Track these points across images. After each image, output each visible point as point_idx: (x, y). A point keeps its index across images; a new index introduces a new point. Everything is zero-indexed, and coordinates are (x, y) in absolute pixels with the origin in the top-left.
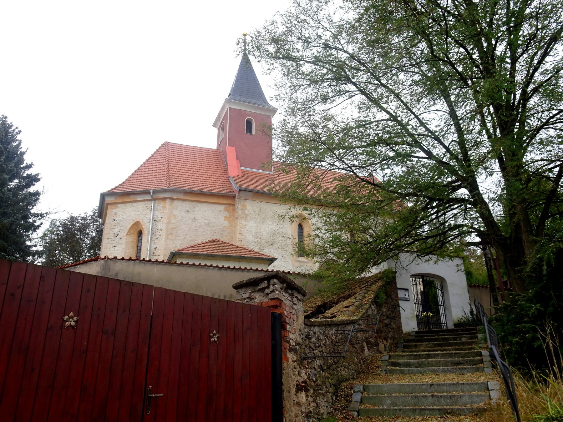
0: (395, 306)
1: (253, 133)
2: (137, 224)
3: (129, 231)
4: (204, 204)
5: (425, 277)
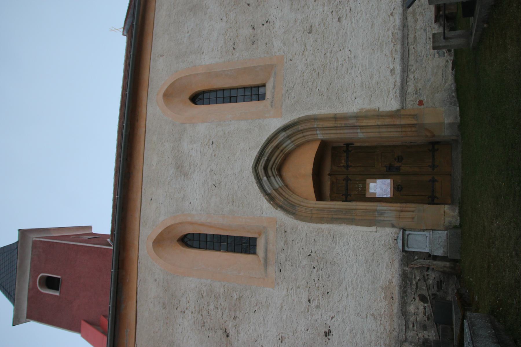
1: (59, 277)
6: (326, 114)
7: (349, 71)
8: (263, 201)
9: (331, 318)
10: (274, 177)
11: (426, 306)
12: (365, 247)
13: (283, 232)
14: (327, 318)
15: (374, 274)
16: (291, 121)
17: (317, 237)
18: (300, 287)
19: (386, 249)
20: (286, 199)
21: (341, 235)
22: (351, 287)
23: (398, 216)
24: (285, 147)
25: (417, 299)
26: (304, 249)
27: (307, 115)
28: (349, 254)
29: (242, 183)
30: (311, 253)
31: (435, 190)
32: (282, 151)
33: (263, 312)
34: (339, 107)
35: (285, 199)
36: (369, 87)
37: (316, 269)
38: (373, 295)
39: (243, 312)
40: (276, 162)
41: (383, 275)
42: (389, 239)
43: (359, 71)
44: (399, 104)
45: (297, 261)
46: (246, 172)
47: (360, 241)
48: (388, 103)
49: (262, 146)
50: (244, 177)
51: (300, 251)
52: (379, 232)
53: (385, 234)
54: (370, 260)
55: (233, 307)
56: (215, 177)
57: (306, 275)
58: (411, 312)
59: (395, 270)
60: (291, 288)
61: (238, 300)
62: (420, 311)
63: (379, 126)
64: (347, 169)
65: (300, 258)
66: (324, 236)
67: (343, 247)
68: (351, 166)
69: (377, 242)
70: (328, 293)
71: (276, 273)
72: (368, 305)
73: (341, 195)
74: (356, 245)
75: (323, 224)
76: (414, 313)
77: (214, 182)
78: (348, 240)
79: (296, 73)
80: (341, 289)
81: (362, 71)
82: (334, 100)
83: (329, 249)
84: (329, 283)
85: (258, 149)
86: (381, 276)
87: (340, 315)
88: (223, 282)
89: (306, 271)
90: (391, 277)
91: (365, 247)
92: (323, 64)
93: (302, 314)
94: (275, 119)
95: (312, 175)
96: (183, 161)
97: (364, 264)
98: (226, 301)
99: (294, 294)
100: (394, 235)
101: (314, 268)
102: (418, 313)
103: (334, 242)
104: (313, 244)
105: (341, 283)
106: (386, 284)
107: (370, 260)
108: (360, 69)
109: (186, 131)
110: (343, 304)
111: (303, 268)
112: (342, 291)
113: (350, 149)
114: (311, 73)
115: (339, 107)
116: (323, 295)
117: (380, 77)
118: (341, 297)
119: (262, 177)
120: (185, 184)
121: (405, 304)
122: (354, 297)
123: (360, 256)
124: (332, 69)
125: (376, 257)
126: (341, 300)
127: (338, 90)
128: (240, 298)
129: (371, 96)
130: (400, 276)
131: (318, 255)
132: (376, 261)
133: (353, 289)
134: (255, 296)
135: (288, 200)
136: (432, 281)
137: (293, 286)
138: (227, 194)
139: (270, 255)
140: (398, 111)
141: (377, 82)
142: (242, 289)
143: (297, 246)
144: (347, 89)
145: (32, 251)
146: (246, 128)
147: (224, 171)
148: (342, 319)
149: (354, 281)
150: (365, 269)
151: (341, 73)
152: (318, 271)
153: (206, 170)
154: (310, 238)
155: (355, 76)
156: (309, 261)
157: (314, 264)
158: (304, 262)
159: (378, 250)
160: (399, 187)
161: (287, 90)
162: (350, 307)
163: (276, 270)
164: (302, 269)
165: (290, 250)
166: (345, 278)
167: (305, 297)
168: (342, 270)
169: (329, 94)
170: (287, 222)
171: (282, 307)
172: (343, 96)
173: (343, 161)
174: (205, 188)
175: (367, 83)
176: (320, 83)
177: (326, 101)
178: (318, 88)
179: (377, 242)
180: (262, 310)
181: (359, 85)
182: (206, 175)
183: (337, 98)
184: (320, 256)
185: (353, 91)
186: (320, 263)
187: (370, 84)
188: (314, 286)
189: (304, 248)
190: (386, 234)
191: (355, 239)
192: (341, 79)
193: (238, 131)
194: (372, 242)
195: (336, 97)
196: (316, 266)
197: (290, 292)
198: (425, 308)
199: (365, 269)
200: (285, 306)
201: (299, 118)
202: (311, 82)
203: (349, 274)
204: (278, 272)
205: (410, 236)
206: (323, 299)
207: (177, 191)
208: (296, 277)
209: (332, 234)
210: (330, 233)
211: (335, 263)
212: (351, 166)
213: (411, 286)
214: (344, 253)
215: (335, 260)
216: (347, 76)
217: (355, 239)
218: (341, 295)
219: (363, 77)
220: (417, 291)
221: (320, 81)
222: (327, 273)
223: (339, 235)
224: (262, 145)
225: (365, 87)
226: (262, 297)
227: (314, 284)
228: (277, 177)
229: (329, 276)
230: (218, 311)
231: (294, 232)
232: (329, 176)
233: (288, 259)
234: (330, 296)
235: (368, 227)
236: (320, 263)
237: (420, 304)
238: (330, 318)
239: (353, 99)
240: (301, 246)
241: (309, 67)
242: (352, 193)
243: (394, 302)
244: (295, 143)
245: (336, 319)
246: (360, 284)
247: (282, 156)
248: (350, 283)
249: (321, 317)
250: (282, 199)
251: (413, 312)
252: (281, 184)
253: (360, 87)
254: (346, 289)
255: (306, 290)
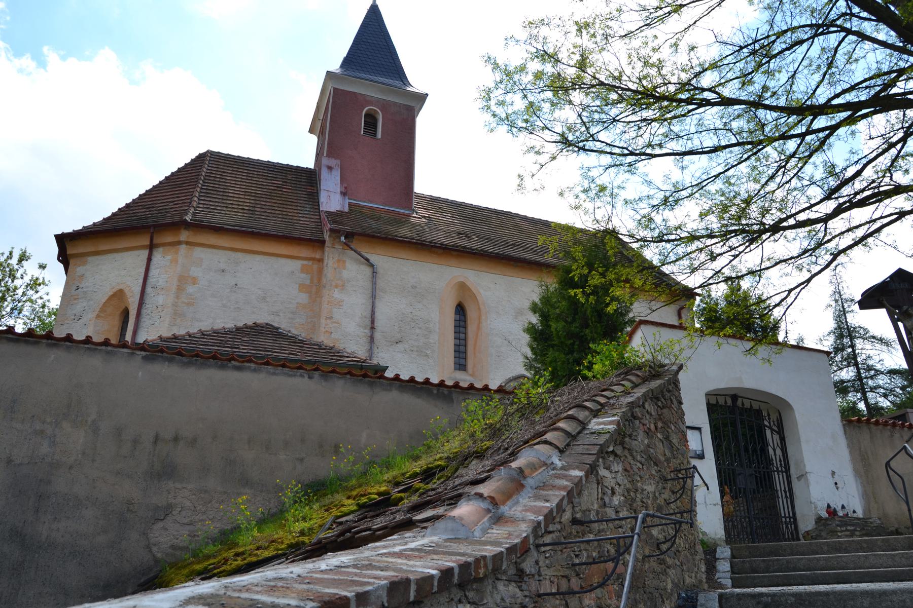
0: (679, 471)
1: (379, 135)
2: (119, 295)
3: (103, 309)
4: (258, 258)
5: (740, 400)
75: (863, 498)
128: (427, 356)
145: (404, 105)
182: (516, 335)
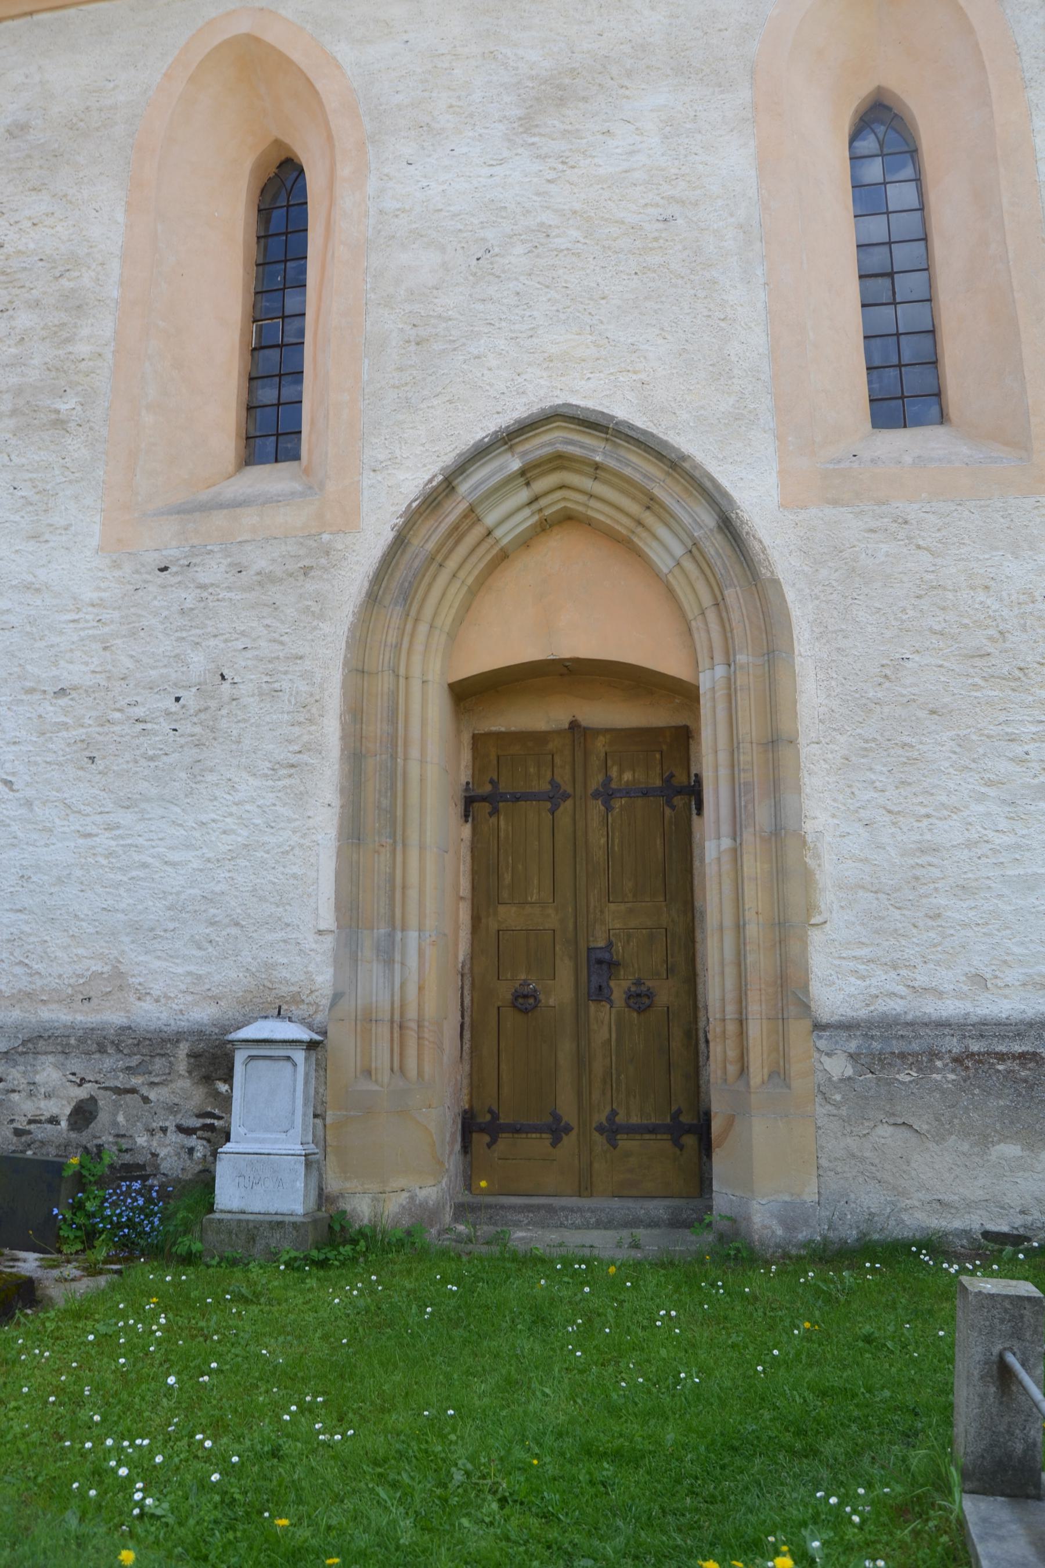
6: (795, 702)
7: (992, 792)
8: (425, 466)
9: (9, 778)
10: (530, 503)
11: (58, 1123)
12: (261, 892)
13: (307, 562)
14: (7, 765)
15: (165, 931)
16: (764, 550)
17: (290, 701)
18: (108, 653)
19: (258, 971)
20: (435, 560)
21: (301, 793)
22: (117, 845)
23: (374, 1015)
24: (655, 537)
25: (82, 1093)
26: (244, 653)
27: (794, 620)
28: (233, 832)
29: (498, 368)
30: (230, 681)
31: (524, 1136)
32: (639, 523)
33: (17, 518)
34: (830, 756)
35: (439, 558)
36: (917, 878)
37: (174, 707)
38: (91, 930)
39: (13, 441)
40: (593, 503)
41: (164, 964)
42: (293, 980)
43: (990, 834)
44: (841, 1011)
45: (199, 632)
46: (542, 382)
47: (281, 869)
48: (844, 963)
49: (653, 435)
50: (525, 377)
51: (237, 639)
52: (316, 942)
53: (311, 968)
54: (212, 911)
55: (28, 402)
56: (519, 249)
57: (152, 672)
58: (36, 1072)
59: (182, 1007)
60: (104, 617)
61: (54, 416)
62: (43, 1104)
63: (739, 927)
64: (596, 795)
65: (212, 642)
66: (296, 730)
67: (258, 806)
68: (609, 809)
69: (280, 935)
70: (92, 759)
71: (156, 555)
72: (59, 912)
73: (495, 778)
74: (266, 856)
76: (34, 1083)
77: (497, 250)
78: (282, 825)
79: (987, 556)
80: (107, 810)
81: (990, 846)
82: (859, 731)
83: (247, 752)
84: (128, 762)
85: (640, 421)
86: (159, 958)
87: (20, 812)
88: (112, 349)
89: (164, 671)
90: (159, 993)
91: (261, 892)
92: (1025, 675)
93: (16, 669)
94: (773, 479)
95: (552, 657)
96: (585, 99)
97: (200, 889)
98: (47, 372)
99: (82, 634)
100: (307, 1001)
101: (178, 699)
102: (36, 1096)
103: (273, 770)
104: (264, 685)
105: (128, 804)
106: (133, 976)
107: (212, 911)
108: (999, 840)
109: (717, 89)
110: (57, 820)
111: (177, 656)
112: (101, 813)
113: (678, 801)
114: (989, 621)
115: (830, 756)
116: (82, 741)
117: (965, 925)
118: (79, 812)
119: (520, 449)
120: (488, 125)
121: (60, 1048)
122: (83, 861)
123: (228, 875)
124: (1002, 717)
125: (224, 933)
126: (68, 811)
127: (904, 745)
128: (59, 423)
129: (876, 892)
130: (163, 1027)
131: (224, 712)
132: (213, 936)
133: (111, 854)
134: (70, 482)
135: (434, 567)
136: (145, 1144)
137: (112, 622)
138: (450, 313)
139: (219, 519)
140: (806, 1007)
141: (939, 915)
142: (91, 429)
143: (254, 624)
144: (909, 784)
146: (733, 358)
147: (548, 287)
148: (8, 821)
149: (136, 857)
150: (183, 897)
151: (984, 755)
152: (167, 715)
153: (548, 208)
154: (286, 673)
155: (970, 820)
156: (200, 676)
157: (189, 698)
158: (198, 662)
159: (250, 941)
160: (531, 1001)
161: (906, 522)
162: (46, 845)
163: (164, 553)
164: (173, 654)
165: (238, 597)
166: (150, 819)
167: (74, 673)
168: (178, 810)
169: (886, 709)
170: (343, 573)
171: (38, 590)
172: (878, 767)
173: (627, 776)
174: (473, 215)
175: (936, 873)
176: (941, 666)
177: (857, 696)
178: (917, 659)
179: (280, 935)
180: (23, 517)
181: (928, 836)
183: (866, 741)
184: (222, 716)
185: (899, 812)
186: (195, 720)
187: (932, 886)
188: (113, 706)
189: (249, 654)
190: (310, 969)
191: (287, 852)
192: (954, 757)
193: (722, 324)
194: (280, 919)
195: (874, 740)
196: (183, 707)
197: (88, 617)
198: (54, 1120)
199: (183, 897)
200: (39, 602)
201: (776, 582)
202: (944, 625)
203: (161, 835)
204: (154, 559)
205: (288, 1065)
206: (69, 745)
207: (459, 97)
208: (142, 634)
209: (304, 757)
210: (309, 750)
211: (199, 778)
212: (609, 809)
213: (122, 1071)
214: (234, 812)
215: (210, 778)
216: (971, 780)
217: (287, 852)
218: (88, 809)
219: (966, 851)
220: (109, 1093)
221: (945, 664)
222: (161, 749)
223: (302, 789)
224: (661, 435)
225: (919, 861)
226: (66, 509)
227: (122, 703)
228: (533, 514)
229: (151, 759)
230: (9, 346)
231: (308, 607)
232: (567, 726)
233: (205, 595)
234: (82, 768)
235: (333, 900)
236: (195, 720)
237: (64, 1102)
238: (7, 774)
239: (862, 813)
240: (254, 640)
241: (1016, 611)
242: (502, 818)
243: (73, 1005)
244: (675, 577)
245: (6, 797)
246: (130, 879)
247: (622, 525)
248: (129, 841)
249: (8, 743)
250: (430, 546)
251: (38, 1079)
252: (505, 535)
253: (920, 842)
254: (108, 828)
255: (98, 676)
